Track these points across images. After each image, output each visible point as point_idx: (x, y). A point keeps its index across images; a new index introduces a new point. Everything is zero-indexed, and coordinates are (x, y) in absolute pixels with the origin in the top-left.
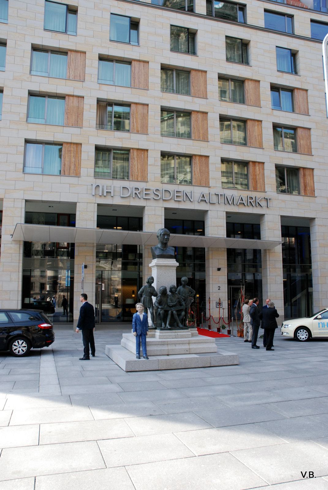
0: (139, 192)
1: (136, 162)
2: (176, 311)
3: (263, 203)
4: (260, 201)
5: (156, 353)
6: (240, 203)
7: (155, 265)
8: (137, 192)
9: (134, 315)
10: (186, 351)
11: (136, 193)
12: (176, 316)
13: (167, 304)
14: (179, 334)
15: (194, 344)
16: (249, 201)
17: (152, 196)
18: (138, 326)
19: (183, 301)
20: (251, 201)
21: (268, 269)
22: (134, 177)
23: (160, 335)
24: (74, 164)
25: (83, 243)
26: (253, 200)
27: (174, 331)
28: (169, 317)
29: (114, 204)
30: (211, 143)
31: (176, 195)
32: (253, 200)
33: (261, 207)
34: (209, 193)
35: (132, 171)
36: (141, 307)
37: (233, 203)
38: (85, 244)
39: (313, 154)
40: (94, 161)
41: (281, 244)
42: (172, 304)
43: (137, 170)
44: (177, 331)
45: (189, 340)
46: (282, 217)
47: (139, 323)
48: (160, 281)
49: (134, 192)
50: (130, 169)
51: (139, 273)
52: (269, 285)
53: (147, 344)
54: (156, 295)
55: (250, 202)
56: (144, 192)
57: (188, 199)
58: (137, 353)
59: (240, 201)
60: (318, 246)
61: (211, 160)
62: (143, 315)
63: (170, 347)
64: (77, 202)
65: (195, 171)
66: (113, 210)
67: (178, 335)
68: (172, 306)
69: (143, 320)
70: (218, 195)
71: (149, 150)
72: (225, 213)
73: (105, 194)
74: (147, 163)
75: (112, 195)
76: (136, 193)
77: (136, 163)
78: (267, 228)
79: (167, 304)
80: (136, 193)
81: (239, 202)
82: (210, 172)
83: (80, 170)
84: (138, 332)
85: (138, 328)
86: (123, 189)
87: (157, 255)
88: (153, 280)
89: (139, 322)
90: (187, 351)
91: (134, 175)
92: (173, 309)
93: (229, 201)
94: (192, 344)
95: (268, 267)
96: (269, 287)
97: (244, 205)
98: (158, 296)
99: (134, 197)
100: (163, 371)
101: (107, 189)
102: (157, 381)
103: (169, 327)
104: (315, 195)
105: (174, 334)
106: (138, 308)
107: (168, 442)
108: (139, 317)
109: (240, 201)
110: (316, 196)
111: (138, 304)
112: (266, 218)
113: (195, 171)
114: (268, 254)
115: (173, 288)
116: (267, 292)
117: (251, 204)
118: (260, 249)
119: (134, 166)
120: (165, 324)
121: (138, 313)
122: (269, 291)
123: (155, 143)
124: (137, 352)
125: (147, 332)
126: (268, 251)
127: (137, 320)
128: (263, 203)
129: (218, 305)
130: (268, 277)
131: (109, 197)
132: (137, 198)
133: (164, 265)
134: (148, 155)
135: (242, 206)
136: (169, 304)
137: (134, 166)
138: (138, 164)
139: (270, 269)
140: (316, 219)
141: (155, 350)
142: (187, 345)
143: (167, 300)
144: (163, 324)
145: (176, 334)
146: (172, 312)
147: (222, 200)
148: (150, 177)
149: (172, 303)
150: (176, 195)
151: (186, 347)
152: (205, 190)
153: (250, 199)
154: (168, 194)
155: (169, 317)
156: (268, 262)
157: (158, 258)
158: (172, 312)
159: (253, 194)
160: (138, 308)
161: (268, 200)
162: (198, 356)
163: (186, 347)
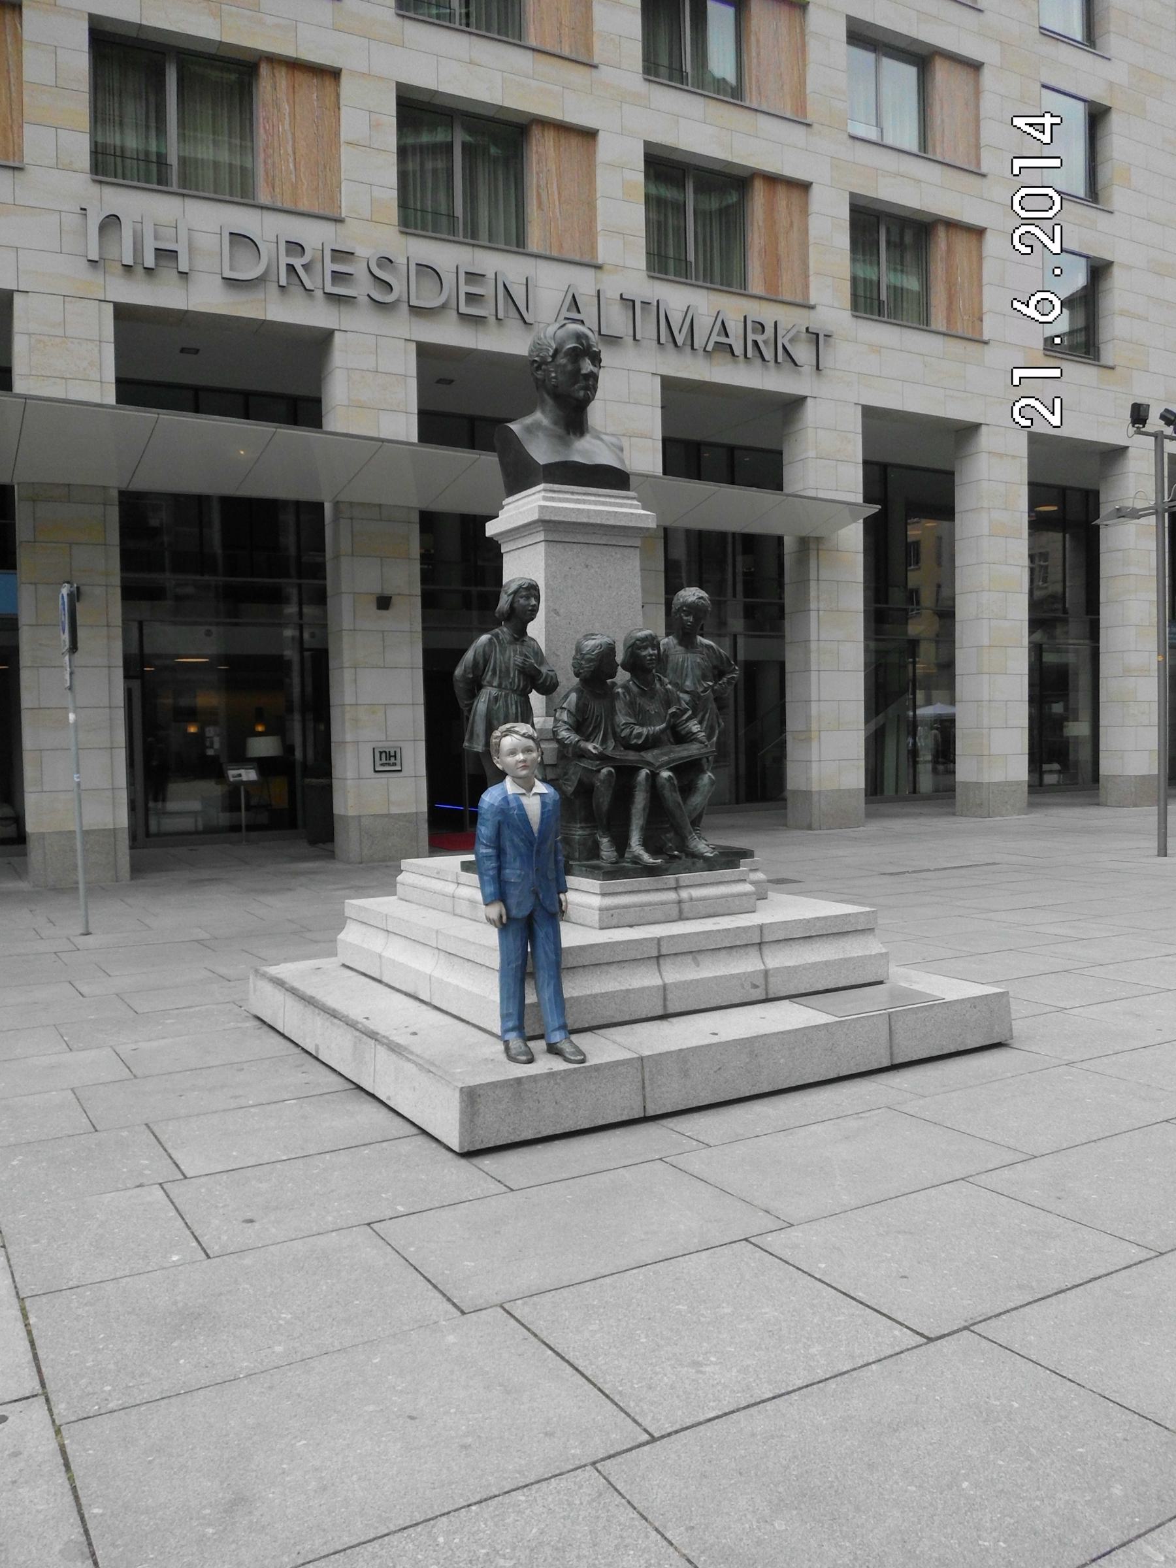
0: (305, 260)
1: (287, 122)
2: (670, 769)
3: (803, 353)
4: (791, 340)
5: (610, 1014)
6: (716, 342)
7: (535, 517)
8: (298, 263)
9: (490, 797)
10: (748, 986)
11: (291, 268)
12: (672, 797)
13: (615, 734)
14: (697, 893)
15: (781, 945)
16: (751, 337)
17: (362, 288)
18: (518, 864)
19: (689, 719)
20: (760, 339)
21: (813, 615)
22: (277, 190)
23: (608, 909)
25: (58, 485)
26: (764, 337)
27: (670, 879)
28: (640, 800)
29: (191, 308)
30: (605, 73)
31: (464, 288)
32: (764, 337)
33: (796, 365)
34: (594, 293)
35: (270, 161)
36: (527, 750)
37: (689, 342)
38: (68, 492)
39: (984, 170)
40: (87, 96)
41: (862, 521)
42: (645, 731)
43: (291, 160)
44: (685, 878)
45: (761, 927)
46: (870, 414)
47: (523, 850)
48: (562, 611)
49: (284, 260)
50: (262, 155)
51: (297, 633)
52: (814, 676)
53: (566, 961)
54: (548, 688)
55: (755, 343)
56: (330, 266)
57: (513, 313)
58: (510, 1024)
59: (718, 335)
60: (986, 531)
61: (605, 148)
62: (537, 800)
63: (675, 974)
64: (12, 291)
65: (539, 195)
66: (183, 350)
67: (691, 899)
68: (652, 743)
69: (540, 831)
70: (633, 302)
71: (343, 72)
72: (658, 380)
73: (150, 261)
74: (337, 134)
75: (183, 266)
76: (291, 268)
77: (287, 127)
78: (812, 453)
79: (615, 734)
80: (292, 266)
81: (715, 338)
82: (599, 202)
83: (21, 136)
84: (512, 901)
85: (512, 873)
86: (231, 242)
87: (546, 466)
88: (538, 599)
89: (517, 840)
90: (755, 986)
91: (277, 182)
92: (648, 756)
93: (676, 333)
94: (581, 970)
95: (813, 606)
96: (814, 687)
97: (729, 355)
98: (561, 690)
99: (283, 282)
100: (665, 1122)
101: (156, 238)
102: (746, 1240)
103: (647, 858)
104: (981, 334)
105: (672, 896)
106: (513, 752)
107: (759, 1543)
108: (521, 807)
109: (718, 335)
110: (985, 338)
111: (509, 732)
112: (811, 413)
113: (539, 195)
114: (813, 554)
115: (646, 648)
116: (808, 701)
117: (758, 355)
118: (779, 532)
119: (276, 144)
120: (621, 844)
121: (510, 786)
122: (814, 696)
123: (372, 42)
124: (505, 1017)
125: (562, 896)
126: (813, 546)
127: (506, 832)
128: (803, 353)
129: (384, 761)
130: (813, 646)
131: (168, 275)
132: (296, 290)
133: (585, 520)
134: (338, 95)
135: (722, 358)
136: (627, 731)
137: (276, 138)
138: (293, 134)
139: (821, 613)
140: (984, 429)
141: (595, 996)
142: (754, 952)
143: (612, 712)
144: (605, 842)
145: (684, 894)
146: (653, 776)
147: (647, 329)
148: (350, 199)
149: (642, 725)
150: (464, 288)
151: (747, 965)
152: (584, 282)
153: (754, 331)
154: (430, 284)
155: (640, 800)
156: (813, 584)
157: (547, 482)
158: (653, 776)
159: (768, 313)
160: (513, 752)
161: (821, 338)
162: (822, 1018)
163: (747, 965)
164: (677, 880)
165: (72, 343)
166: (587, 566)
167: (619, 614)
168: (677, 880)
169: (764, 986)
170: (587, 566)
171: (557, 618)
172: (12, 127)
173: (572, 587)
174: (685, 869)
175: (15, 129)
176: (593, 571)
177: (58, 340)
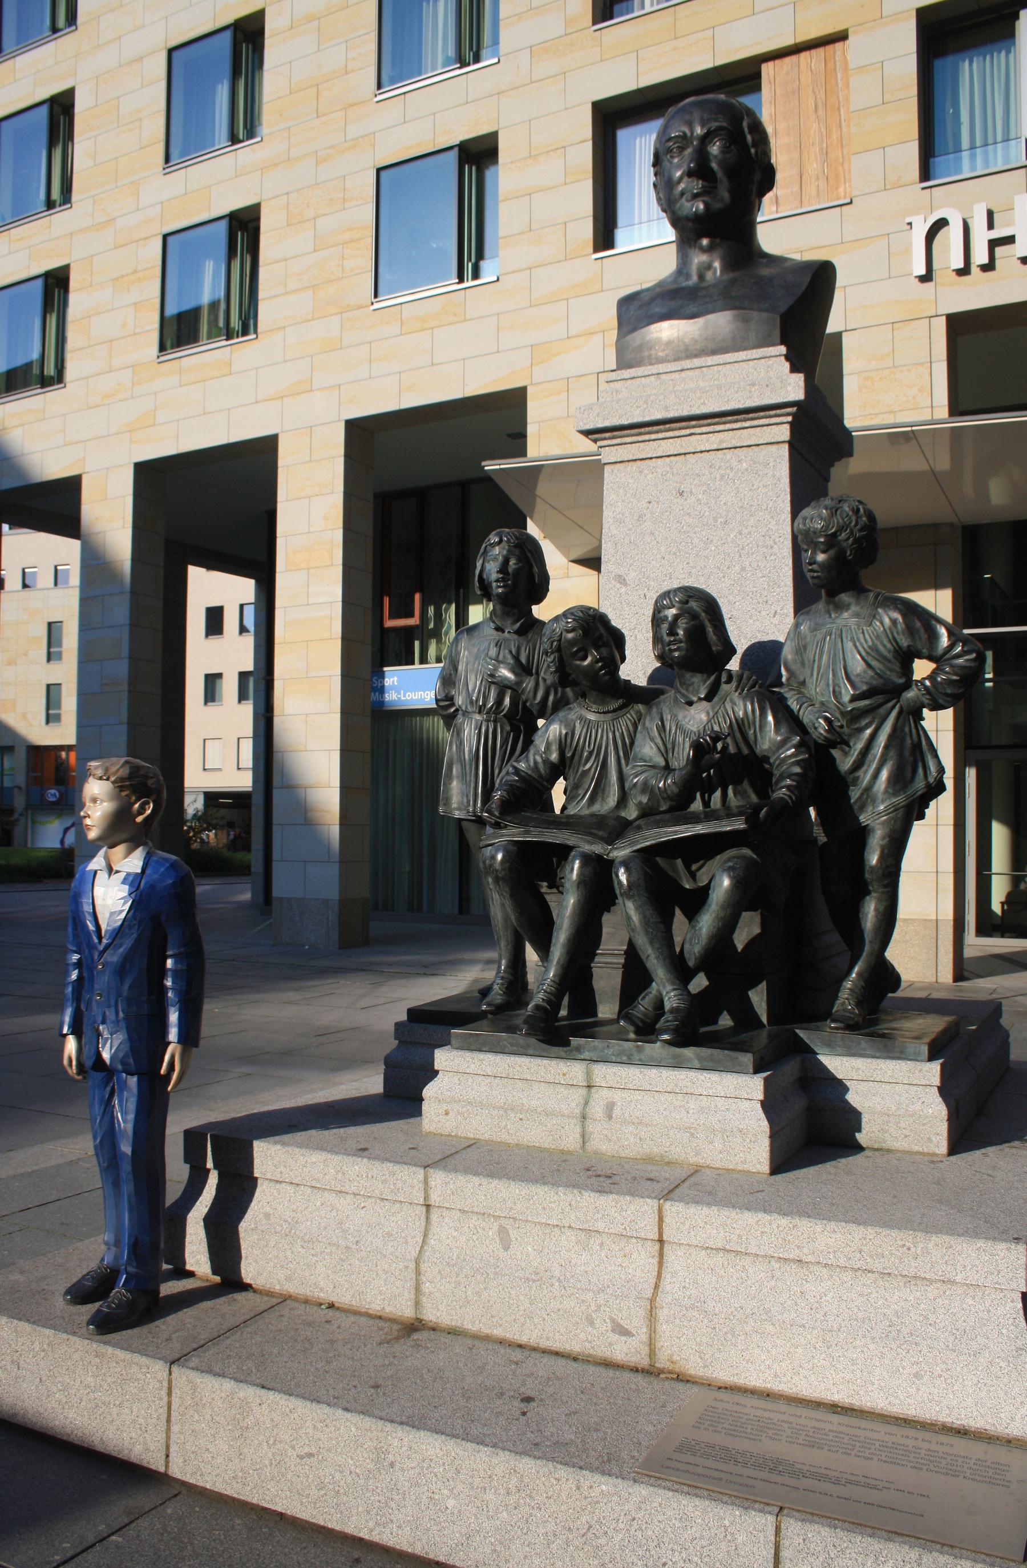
24: (821, 149)
48: (631, 576)
90: (625, 1332)
101: (991, 226)
164: (589, 1075)
165: (901, 372)
166: (681, 494)
167: (743, 569)
168: (589, 1075)
169: (644, 1337)
170: (681, 494)
171: (623, 590)
172: (842, 164)
173: (652, 533)
174: (620, 1054)
175: (846, 165)
176: (692, 500)
177: (887, 371)
